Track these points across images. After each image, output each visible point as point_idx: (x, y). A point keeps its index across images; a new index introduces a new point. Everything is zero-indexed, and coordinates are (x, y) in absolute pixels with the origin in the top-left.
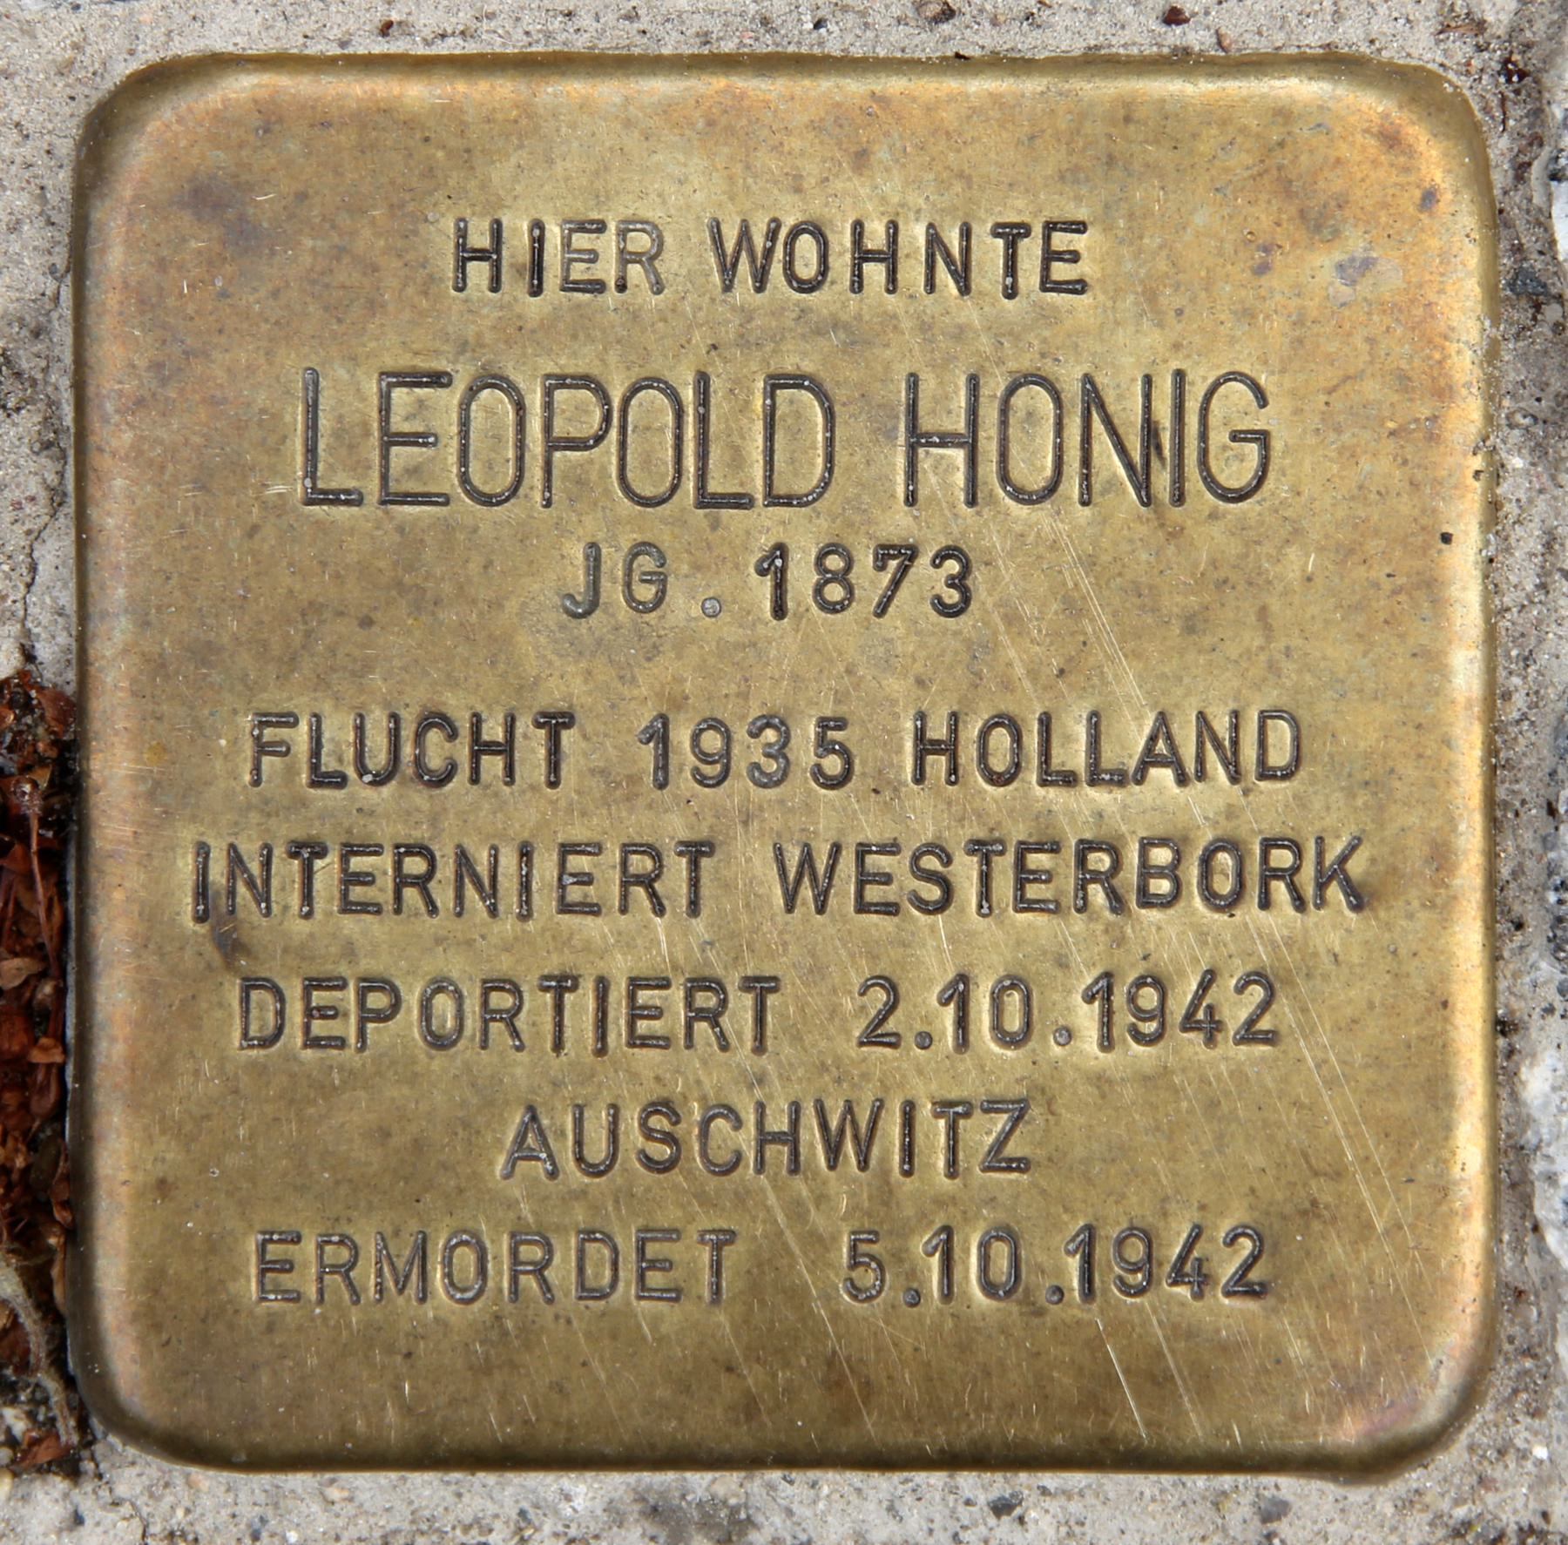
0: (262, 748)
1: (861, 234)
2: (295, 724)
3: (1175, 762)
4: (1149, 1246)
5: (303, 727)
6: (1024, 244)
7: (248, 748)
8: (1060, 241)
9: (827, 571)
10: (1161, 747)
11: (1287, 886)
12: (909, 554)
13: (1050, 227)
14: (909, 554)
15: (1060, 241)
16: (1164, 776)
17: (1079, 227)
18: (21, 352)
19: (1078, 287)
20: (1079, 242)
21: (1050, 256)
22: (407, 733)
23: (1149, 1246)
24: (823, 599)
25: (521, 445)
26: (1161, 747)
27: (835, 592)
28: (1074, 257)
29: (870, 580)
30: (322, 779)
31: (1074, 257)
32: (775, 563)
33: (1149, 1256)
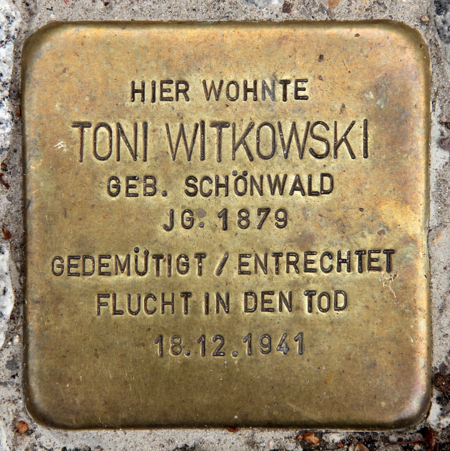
0: (100, 304)
1: (340, 254)
2: (109, 297)
3: (301, 189)
4: (270, 340)
5: (111, 298)
6: (288, 87)
7: (96, 304)
8: (300, 85)
9: (241, 217)
10: (298, 185)
11: (359, 257)
12: (268, 210)
13: (297, 81)
14: (268, 210)
15: (300, 85)
16: (298, 193)
17: (306, 81)
18: (14, 179)
19: (305, 98)
20: (305, 85)
21: (297, 89)
22: (143, 299)
23: (270, 340)
24: (241, 225)
25: (111, 141)
26: (298, 185)
27: (244, 223)
28: (304, 89)
29: (254, 219)
30: (116, 312)
31: (304, 89)
32: (224, 214)
33: (270, 343)
